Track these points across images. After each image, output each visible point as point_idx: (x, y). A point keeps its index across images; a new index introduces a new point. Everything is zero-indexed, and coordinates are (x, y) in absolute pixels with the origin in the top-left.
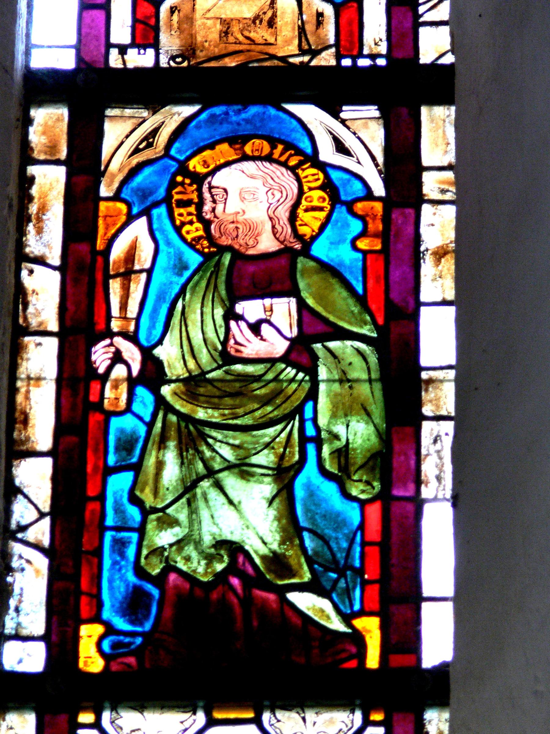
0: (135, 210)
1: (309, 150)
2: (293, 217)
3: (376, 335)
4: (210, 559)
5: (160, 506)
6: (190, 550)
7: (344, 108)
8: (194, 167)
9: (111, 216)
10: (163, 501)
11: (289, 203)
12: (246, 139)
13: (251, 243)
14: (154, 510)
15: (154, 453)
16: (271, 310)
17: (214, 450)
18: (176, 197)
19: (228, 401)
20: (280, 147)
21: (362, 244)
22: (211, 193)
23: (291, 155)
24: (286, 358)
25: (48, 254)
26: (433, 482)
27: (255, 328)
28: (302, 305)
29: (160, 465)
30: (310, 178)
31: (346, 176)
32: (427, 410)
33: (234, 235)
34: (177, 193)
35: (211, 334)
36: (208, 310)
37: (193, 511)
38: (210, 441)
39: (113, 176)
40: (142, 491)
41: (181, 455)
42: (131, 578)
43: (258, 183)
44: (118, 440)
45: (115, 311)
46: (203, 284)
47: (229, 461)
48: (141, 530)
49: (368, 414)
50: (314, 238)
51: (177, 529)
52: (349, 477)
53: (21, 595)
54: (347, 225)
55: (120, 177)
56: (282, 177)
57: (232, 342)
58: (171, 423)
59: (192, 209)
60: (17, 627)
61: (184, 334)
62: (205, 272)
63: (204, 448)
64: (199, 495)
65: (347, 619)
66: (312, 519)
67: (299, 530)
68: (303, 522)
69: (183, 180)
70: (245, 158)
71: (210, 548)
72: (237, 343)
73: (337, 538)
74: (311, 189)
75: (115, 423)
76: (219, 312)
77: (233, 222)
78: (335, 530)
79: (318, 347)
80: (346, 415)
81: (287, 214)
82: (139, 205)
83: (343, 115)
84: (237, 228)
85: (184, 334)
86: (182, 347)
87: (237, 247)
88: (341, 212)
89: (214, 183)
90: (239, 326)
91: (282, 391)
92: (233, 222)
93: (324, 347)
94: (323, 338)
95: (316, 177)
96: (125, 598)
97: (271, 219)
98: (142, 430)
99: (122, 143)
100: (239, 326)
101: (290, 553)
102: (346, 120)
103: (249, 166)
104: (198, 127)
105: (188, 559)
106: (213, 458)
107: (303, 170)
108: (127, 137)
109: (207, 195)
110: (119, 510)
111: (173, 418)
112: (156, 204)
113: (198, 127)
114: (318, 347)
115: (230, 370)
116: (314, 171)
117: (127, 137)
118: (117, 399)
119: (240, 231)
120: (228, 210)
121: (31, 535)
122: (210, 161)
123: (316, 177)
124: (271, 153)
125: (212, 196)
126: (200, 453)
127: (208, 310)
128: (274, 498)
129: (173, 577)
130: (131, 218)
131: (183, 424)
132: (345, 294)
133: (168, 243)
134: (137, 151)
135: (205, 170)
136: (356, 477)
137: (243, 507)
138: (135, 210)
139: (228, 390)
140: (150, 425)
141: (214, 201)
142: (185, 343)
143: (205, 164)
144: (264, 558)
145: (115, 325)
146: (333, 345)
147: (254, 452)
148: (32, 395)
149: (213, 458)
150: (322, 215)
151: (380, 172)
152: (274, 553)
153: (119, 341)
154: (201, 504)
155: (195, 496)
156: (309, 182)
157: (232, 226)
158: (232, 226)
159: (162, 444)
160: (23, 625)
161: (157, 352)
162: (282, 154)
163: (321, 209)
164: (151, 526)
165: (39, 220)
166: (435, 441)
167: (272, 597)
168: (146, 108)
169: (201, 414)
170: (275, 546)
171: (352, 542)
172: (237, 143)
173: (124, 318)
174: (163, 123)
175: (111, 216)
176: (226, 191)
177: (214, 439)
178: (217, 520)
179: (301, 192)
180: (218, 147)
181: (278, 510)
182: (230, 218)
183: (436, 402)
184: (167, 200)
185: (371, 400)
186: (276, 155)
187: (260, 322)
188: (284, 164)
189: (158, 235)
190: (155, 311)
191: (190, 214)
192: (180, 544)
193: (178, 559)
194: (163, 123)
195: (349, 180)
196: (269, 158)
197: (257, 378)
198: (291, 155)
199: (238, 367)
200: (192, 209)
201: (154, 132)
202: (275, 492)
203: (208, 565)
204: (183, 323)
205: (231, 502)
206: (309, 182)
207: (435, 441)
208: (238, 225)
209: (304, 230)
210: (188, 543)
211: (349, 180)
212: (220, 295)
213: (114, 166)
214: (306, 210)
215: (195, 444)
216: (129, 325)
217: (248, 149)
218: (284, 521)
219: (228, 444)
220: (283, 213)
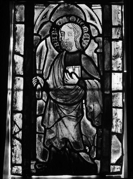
0: (42, 38)
1: (84, 20)
2: (81, 41)
3: (100, 79)
4: (61, 143)
5: (49, 127)
6: (56, 140)
7: (93, 5)
8: (57, 24)
9: (36, 40)
10: (50, 126)
11: (80, 37)
12: (70, 16)
13: (70, 49)
14: (48, 128)
15: (48, 112)
16: (75, 70)
17: (61, 111)
18: (53, 34)
19: (65, 97)
20: (78, 19)
21: (98, 51)
22: (61, 33)
23: (81, 22)
24: (78, 84)
25: (21, 51)
26: (115, 127)
27: (71, 75)
28: (82, 68)
29: (49, 115)
30: (85, 29)
31: (94, 28)
32: (114, 105)
33: (66, 46)
34: (53, 33)
35: (60, 76)
36: (59, 69)
37: (57, 129)
38: (61, 108)
39: (37, 26)
40: (45, 123)
41: (54, 112)
42: (42, 147)
43: (72, 30)
44: (39, 107)
45: (37, 68)
46: (59, 61)
47: (65, 114)
48: (45, 134)
49: (98, 102)
50: (86, 48)
51: (53, 134)
52: (94, 120)
53: (16, 152)
54: (94, 45)
55: (39, 27)
56: (78, 29)
57: (65, 79)
58: (52, 103)
59: (56, 38)
60: (15, 161)
61: (54, 76)
62: (59, 58)
63: (59, 110)
64: (58, 124)
65: (93, 160)
66: (85, 133)
67: (82, 135)
68: (83, 133)
69: (54, 29)
70: (70, 22)
71: (61, 140)
72: (66, 79)
73: (90, 137)
74: (85, 33)
75: (38, 101)
76: (62, 69)
77: (66, 42)
78: (90, 135)
79: (86, 81)
80: (93, 102)
81: (79, 40)
82: (43, 36)
83: (93, 8)
84: (67, 44)
85: (54, 76)
86: (53, 80)
87: (67, 50)
88: (93, 41)
89: (62, 30)
90: (67, 74)
91: (78, 93)
92: (66, 42)
93: (88, 81)
94: (88, 79)
95: (86, 29)
96: (41, 152)
97: (75, 41)
98: (44, 104)
99: (39, 16)
100: (67, 74)
101: (79, 141)
102: (93, 9)
103: (70, 25)
104: (57, 12)
105: (56, 143)
106: (61, 113)
107: (83, 27)
108: (40, 14)
109: (60, 34)
110: (40, 128)
111: (52, 101)
112: (47, 36)
113: (57, 12)
114: (86, 81)
115: (65, 87)
116: (86, 27)
117: (40, 14)
118: (39, 95)
119: (68, 45)
120: (65, 39)
121: (17, 136)
122: (61, 22)
123: (86, 29)
124: (76, 21)
125: (61, 34)
126: (58, 111)
127: (59, 69)
128: (76, 126)
129: (53, 148)
130: (41, 41)
131: (54, 103)
132: (93, 66)
133: (50, 48)
134: (42, 19)
135: (60, 25)
136: (96, 120)
137: (69, 128)
138: (42, 38)
139: (64, 93)
140: (46, 103)
141: (62, 36)
142: (54, 78)
143: (60, 23)
144: (73, 143)
145: (37, 72)
146: (90, 81)
147: (71, 112)
148: (17, 94)
149: (61, 113)
150: (88, 41)
151: (101, 26)
152: (76, 141)
153: (38, 77)
154: (59, 127)
155: (57, 124)
156: (85, 30)
157: (66, 43)
158: (66, 43)
159: (49, 110)
160: (17, 161)
161: (47, 81)
162: (78, 22)
163: (88, 39)
164: (47, 133)
165: (18, 41)
166: (115, 115)
167: (76, 154)
168: (44, 6)
169: (58, 100)
170: (76, 139)
171: (94, 138)
172: (68, 17)
173: (39, 70)
174: (49, 10)
175: (36, 40)
176: (64, 32)
177: (61, 107)
178: (63, 132)
179: (83, 34)
180: (63, 18)
181: (77, 129)
182: (66, 41)
183: (117, 102)
184: (50, 35)
185: (99, 98)
186: (77, 22)
187: (72, 73)
188: (79, 24)
189: (48, 46)
190: (47, 68)
191: (56, 39)
192: (54, 138)
193: (54, 143)
194: (49, 10)
195: (95, 30)
196: (75, 23)
197: (71, 90)
198: (81, 22)
199: (67, 87)
200: (56, 38)
201: (47, 13)
202: (76, 124)
203: (60, 145)
204: (54, 74)
205: (66, 127)
206: (85, 30)
207: (115, 115)
208: (68, 43)
209: (84, 45)
210: (56, 138)
211: (95, 30)
212: (62, 65)
213: (37, 23)
214: (84, 39)
215: (57, 109)
216: (41, 72)
217: (71, 19)
218: (78, 132)
219: (65, 109)
220: (78, 40)
